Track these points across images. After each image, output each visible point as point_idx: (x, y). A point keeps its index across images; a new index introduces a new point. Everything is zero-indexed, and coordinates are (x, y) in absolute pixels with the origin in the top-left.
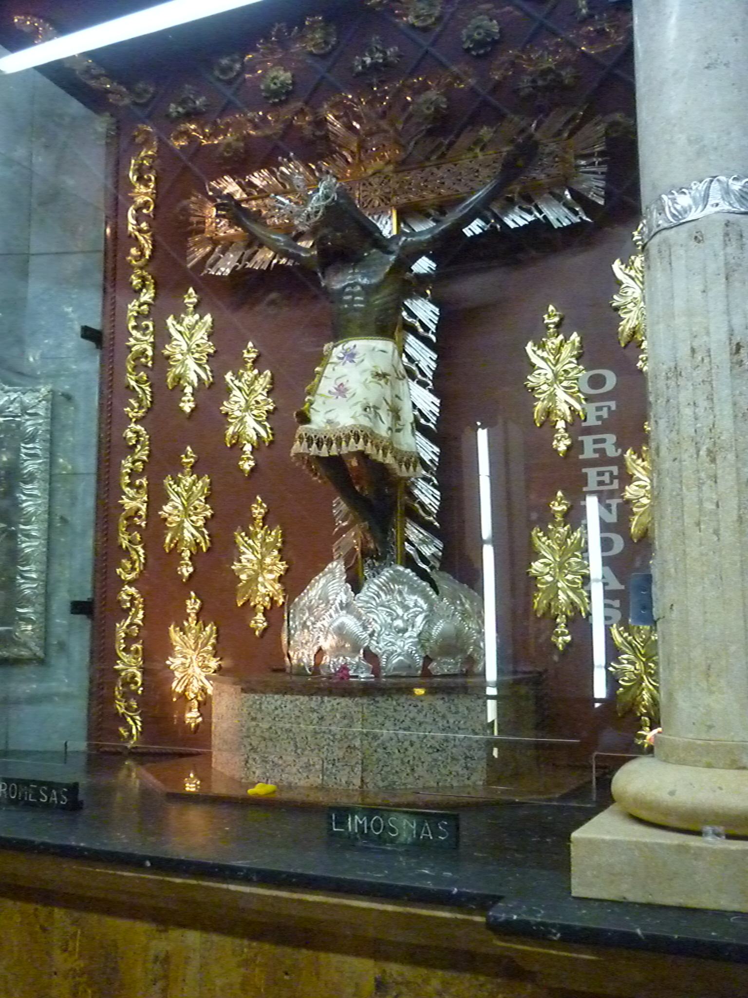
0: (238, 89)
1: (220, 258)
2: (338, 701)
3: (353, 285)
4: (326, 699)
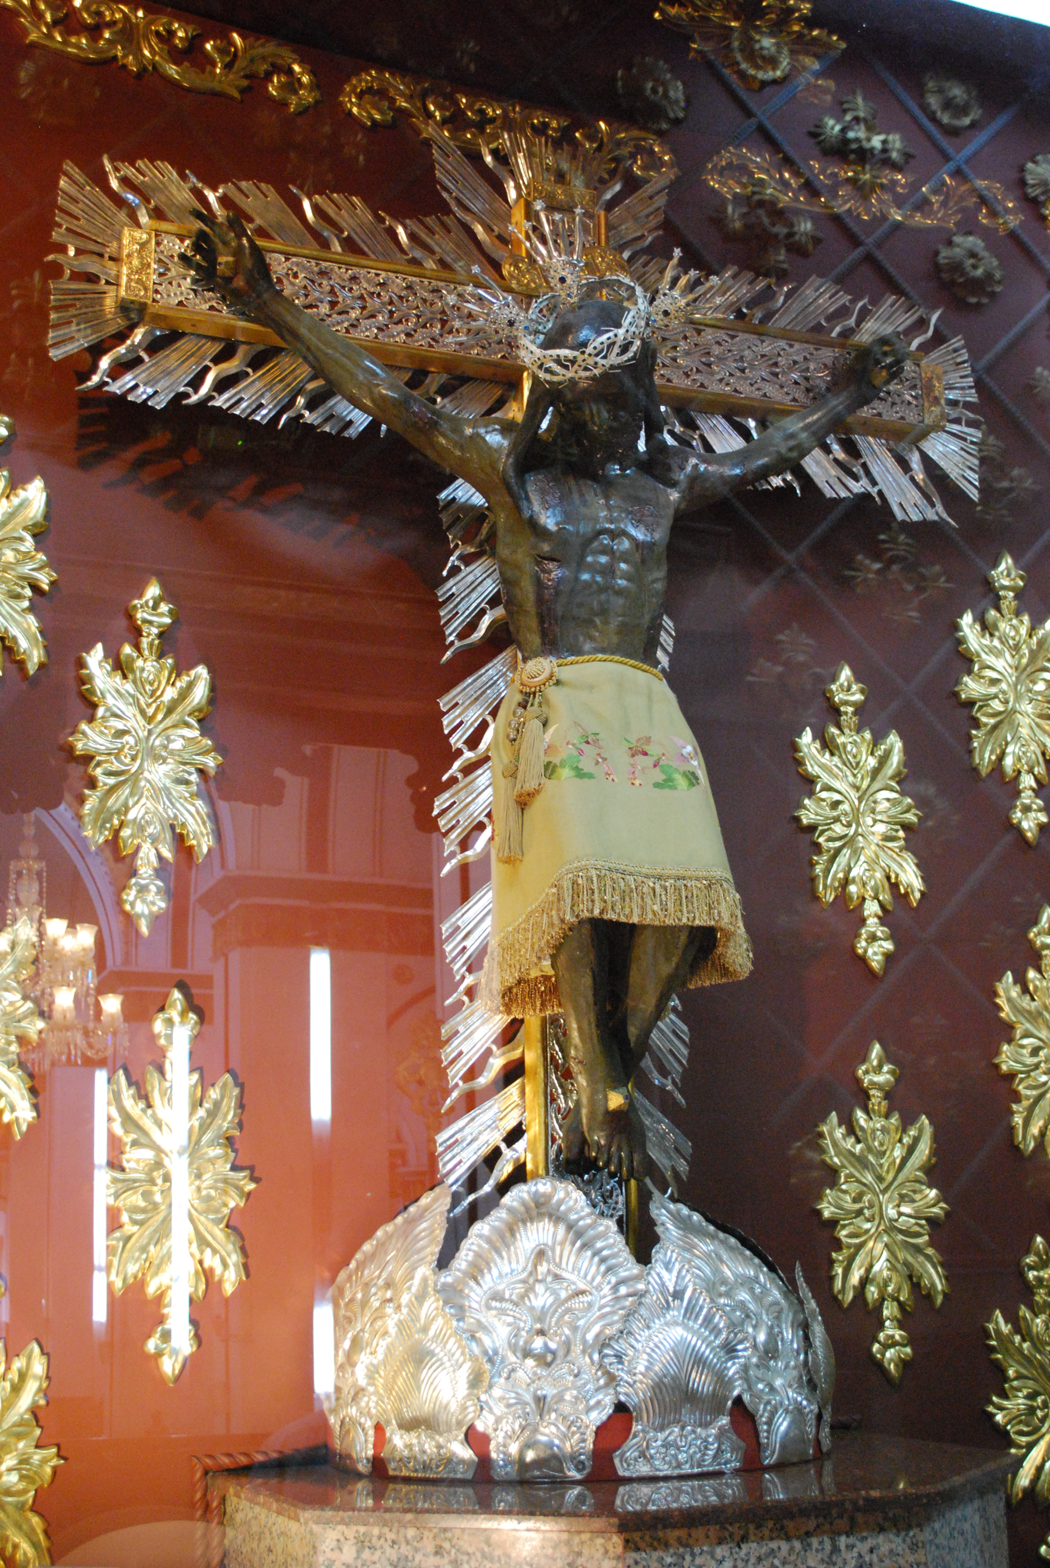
0: (695, 300)
1: (139, 361)
2: (870, 1542)
3: (614, 535)
4: (843, 1541)
